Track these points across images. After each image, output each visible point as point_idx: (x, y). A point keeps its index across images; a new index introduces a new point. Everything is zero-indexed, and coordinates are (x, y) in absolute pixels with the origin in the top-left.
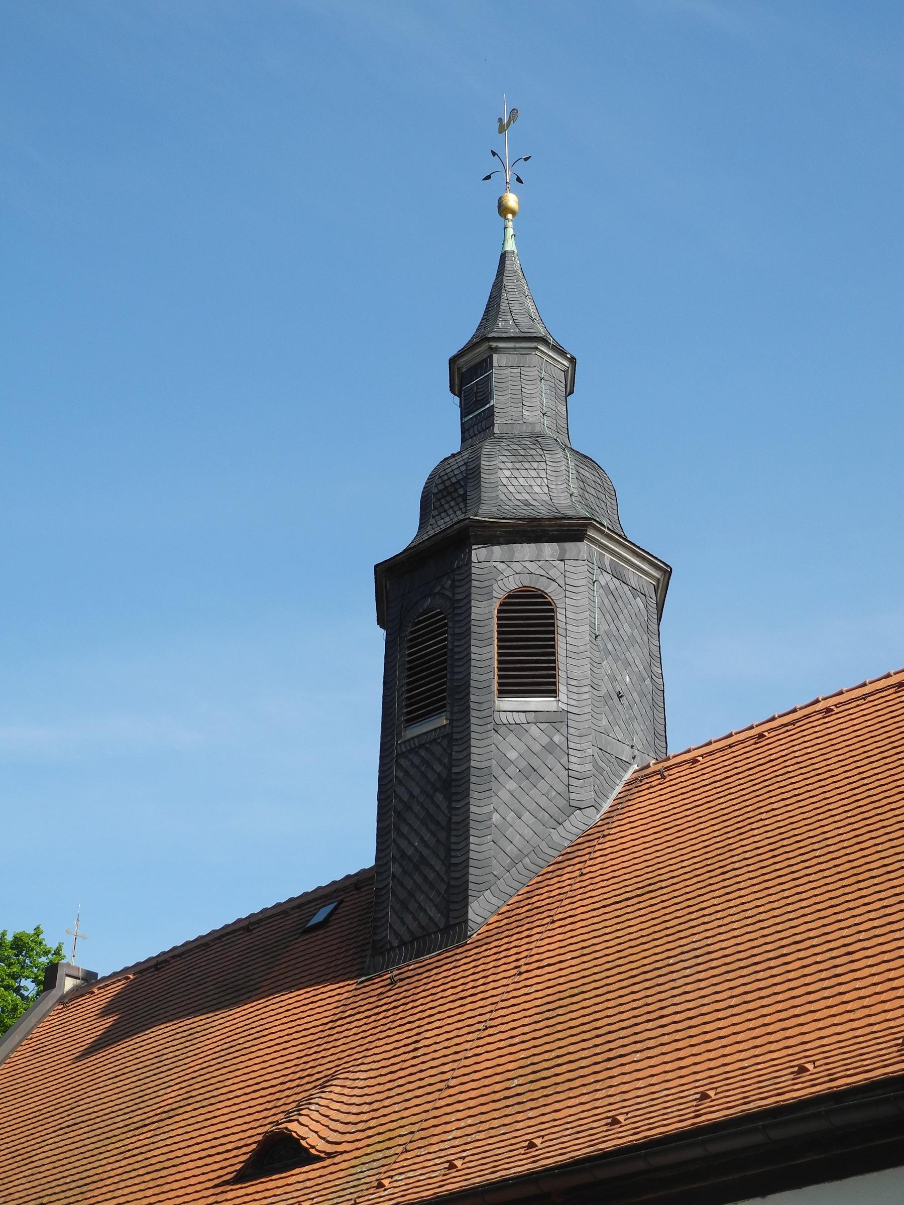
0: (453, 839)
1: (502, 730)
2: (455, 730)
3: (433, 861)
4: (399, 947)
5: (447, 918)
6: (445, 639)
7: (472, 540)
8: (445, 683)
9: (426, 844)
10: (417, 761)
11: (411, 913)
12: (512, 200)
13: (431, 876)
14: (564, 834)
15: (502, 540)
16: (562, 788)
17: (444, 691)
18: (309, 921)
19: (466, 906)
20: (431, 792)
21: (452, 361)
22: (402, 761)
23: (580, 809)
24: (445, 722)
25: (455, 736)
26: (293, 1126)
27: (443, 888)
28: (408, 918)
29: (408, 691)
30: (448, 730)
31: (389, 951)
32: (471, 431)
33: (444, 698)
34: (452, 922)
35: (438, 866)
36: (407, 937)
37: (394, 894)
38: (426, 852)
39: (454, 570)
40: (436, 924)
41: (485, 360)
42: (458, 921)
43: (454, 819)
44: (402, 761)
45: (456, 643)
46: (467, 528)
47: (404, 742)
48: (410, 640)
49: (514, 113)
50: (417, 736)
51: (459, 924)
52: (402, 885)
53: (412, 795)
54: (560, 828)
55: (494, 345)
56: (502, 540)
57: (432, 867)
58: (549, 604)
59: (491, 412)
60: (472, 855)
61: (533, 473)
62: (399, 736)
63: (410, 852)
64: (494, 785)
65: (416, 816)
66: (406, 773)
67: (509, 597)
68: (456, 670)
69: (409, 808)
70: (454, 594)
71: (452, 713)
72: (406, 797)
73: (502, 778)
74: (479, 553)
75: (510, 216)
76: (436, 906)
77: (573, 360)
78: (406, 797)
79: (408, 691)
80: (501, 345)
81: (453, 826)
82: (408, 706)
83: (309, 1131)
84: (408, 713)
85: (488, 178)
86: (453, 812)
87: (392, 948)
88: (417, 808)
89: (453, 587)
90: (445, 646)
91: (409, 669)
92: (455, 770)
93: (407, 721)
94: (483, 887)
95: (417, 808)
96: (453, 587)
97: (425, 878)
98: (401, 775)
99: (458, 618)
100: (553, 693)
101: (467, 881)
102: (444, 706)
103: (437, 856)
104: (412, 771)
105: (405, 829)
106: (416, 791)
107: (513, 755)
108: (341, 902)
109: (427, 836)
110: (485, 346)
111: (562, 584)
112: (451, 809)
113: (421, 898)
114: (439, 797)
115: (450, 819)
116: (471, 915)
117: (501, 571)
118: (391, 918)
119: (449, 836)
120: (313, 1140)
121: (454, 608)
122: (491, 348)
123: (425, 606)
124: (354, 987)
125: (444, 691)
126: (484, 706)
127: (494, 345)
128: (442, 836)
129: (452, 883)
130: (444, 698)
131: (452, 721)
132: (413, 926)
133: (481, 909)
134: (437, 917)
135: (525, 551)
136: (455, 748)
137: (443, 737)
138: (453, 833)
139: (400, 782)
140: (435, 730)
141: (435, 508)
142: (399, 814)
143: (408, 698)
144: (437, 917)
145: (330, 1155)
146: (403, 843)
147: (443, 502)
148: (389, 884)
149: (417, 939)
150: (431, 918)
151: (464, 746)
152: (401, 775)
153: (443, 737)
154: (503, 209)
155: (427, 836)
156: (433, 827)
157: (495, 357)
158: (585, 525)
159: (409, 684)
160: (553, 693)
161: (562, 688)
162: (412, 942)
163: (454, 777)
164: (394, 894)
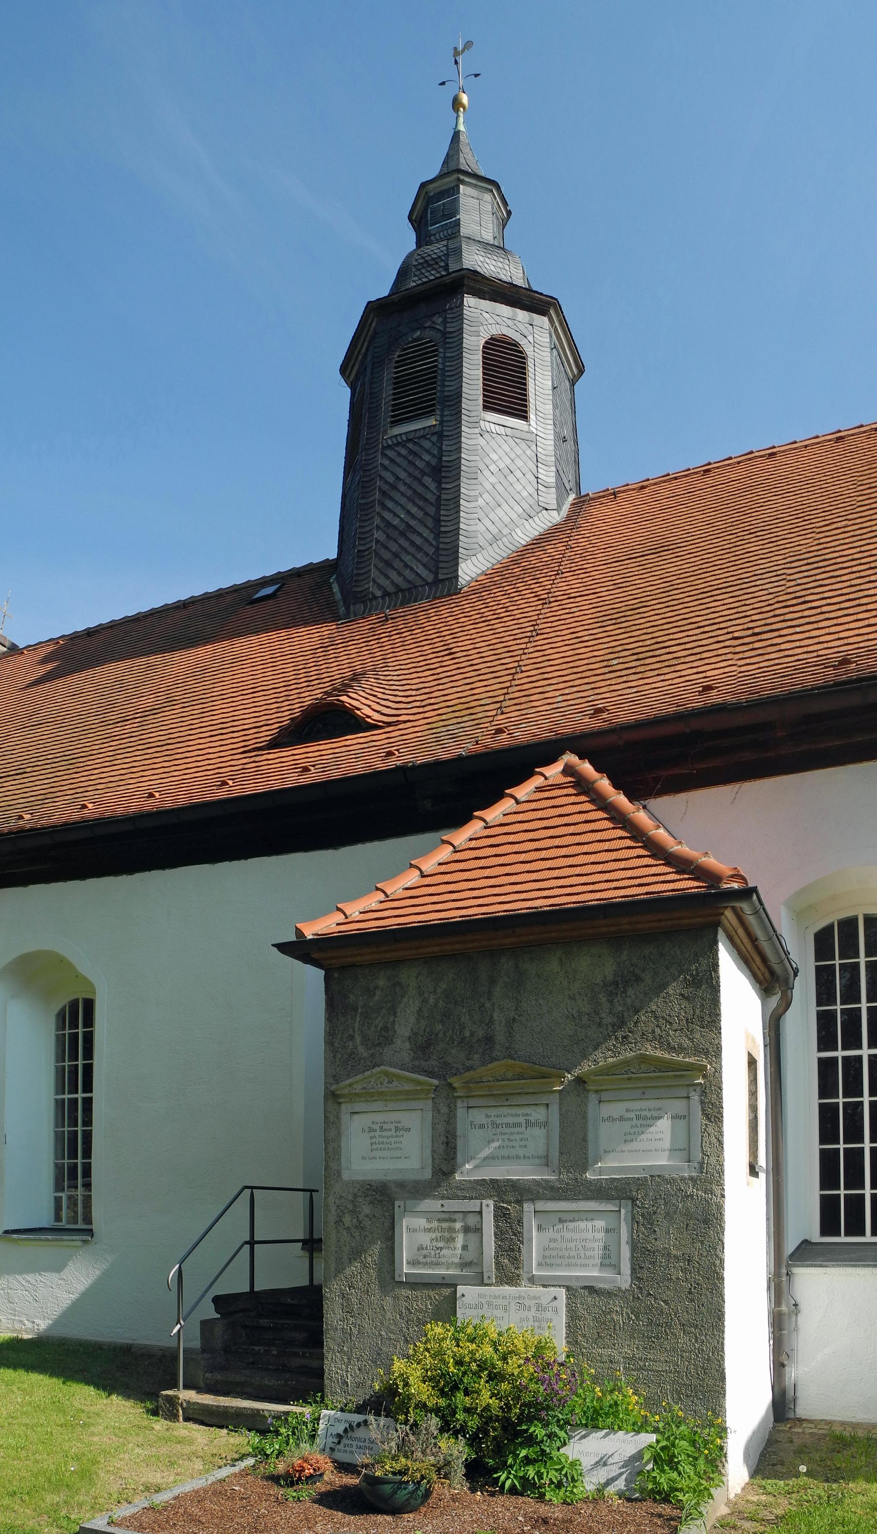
0: (442, 512)
1: (486, 435)
2: (445, 428)
3: (421, 529)
4: (383, 597)
5: (436, 574)
6: (436, 361)
7: (465, 289)
8: (435, 394)
9: (413, 516)
10: (403, 452)
11: (395, 570)
12: (465, 99)
13: (418, 541)
14: (534, 525)
15: (487, 296)
16: (532, 490)
17: (434, 399)
18: (258, 592)
19: (457, 564)
20: (419, 476)
21: (423, 185)
22: (388, 452)
23: (547, 509)
24: (434, 423)
25: (445, 433)
26: (344, 698)
27: (431, 551)
28: (393, 575)
29: (394, 400)
30: (437, 429)
31: (371, 600)
32: (437, 236)
33: (434, 405)
34: (441, 577)
35: (426, 533)
36: (391, 589)
37: (377, 554)
38: (413, 523)
39: (446, 311)
40: (423, 579)
41: (453, 188)
42: (449, 576)
43: (444, 497)
44: (388, 452)
45: (447, 364)
46: (462, 278)
47: (391, 438)
48: (397, 362)
49: (468, 45)
50: (405, 433)
51: (450, 579)
52: (386, 548)
53: (398, 478)
54: (531, 521)
55: (462, 177)
56: (487, 296)
57: (420, 534)
58: (521, 352)
59: (457, 224)
60: (462, 526)
61: (500, 265)
62: (385, 432)
63: (396, 522)
64: (480, 477)
65: (402, 494)
66: (392, 461)
67: (491, 339)
68: (446, 383)
69: (394, 487)
70: (445, 328)
71: (442, 416)
72: (391, 479)
73: (486, 473)
74: (469, 301)
75: (462, 109)
76: (424, 565)
77: (509, 213)
78: (391, 479)
79: (394, 400)
80: (467, 179)
81: (442, 502)
82: (393, 411)
83: (360, 702)
84: (393, 416)
85: (443, 84)
86: (443, 492)
87: (375, 598)
88: (403, 488)
89: (445, 322)
90: (436, 366)
91: (395, 384)
92: (444, 459)
93: (392, 422)
94: (470, 552)
95: (403, 488)
96: (445, 322)
97: (413, 543)
98: (386, 462)
99: (448, 346)
100: (525, 418)
101: (458, 546)
102: (434, 411)
103: (425, 526)
104: (399, 460)
105: (390, 504)
106: (403, 475)
107: (495, 457)
108: (283, 584)
109: (414, 510)
110: (455, 176)
111: (532, 341)
112: (440, 489)
113: (407, 558)
114: (427, 480)
115: (439, 497)
116: (460, 573)
117: (484, 320)
118: (374, 573)
119: (438, 509)
120: (367, 711)
121: (446, 338)
122: (459, 179)
123: (415, 336)
124: (334, 627)
125: (434, 399)
126: (473, 414)
127: (462, 177)
128: (431, 510)
129: (441, 546)
130: (434, 405)
131: (442, 422)
132: (398, 580)
133: (469, 570)
134: (424, 573)
135: (505, 310)
136: (445, 443)
137: (433, 434)
138: (442, 507)
139: (386, 468)
140: (424, 428)
141: (415, 276)
142: (384, 493)
143: (393, 405)
144: (424, 573)
145: (389, 724)
146: (388, 516)
147: (423, 271)
148: (372, 547)
149: (402, 590)
150: (418, 574)
151: (456, 441)
152: (386, 462)
153: (433, 434)
154: (456, 104)
155: (414, 510)
156: (421, 503)
157: (461, 187)
158: (549, 304)
159: (394, 394)
160: (525, 418)
161: (532, 416)
162: (396, 593)
163: (444, 464)
164: (377, 554)
